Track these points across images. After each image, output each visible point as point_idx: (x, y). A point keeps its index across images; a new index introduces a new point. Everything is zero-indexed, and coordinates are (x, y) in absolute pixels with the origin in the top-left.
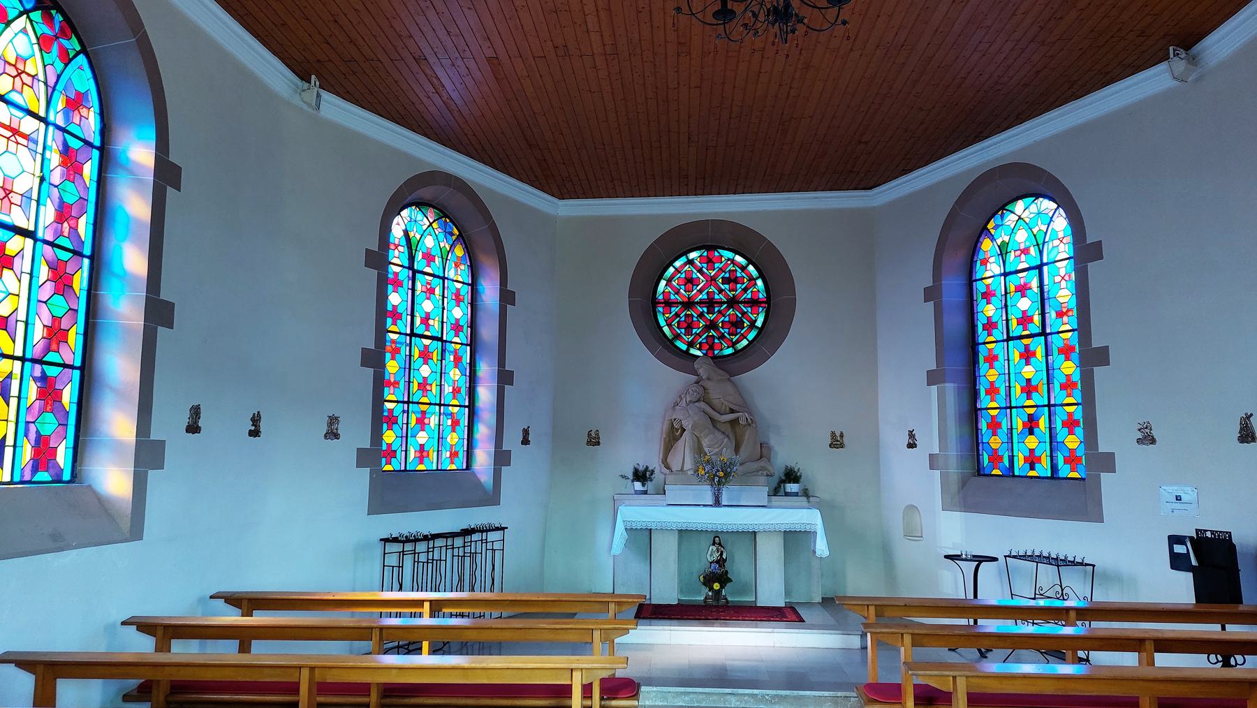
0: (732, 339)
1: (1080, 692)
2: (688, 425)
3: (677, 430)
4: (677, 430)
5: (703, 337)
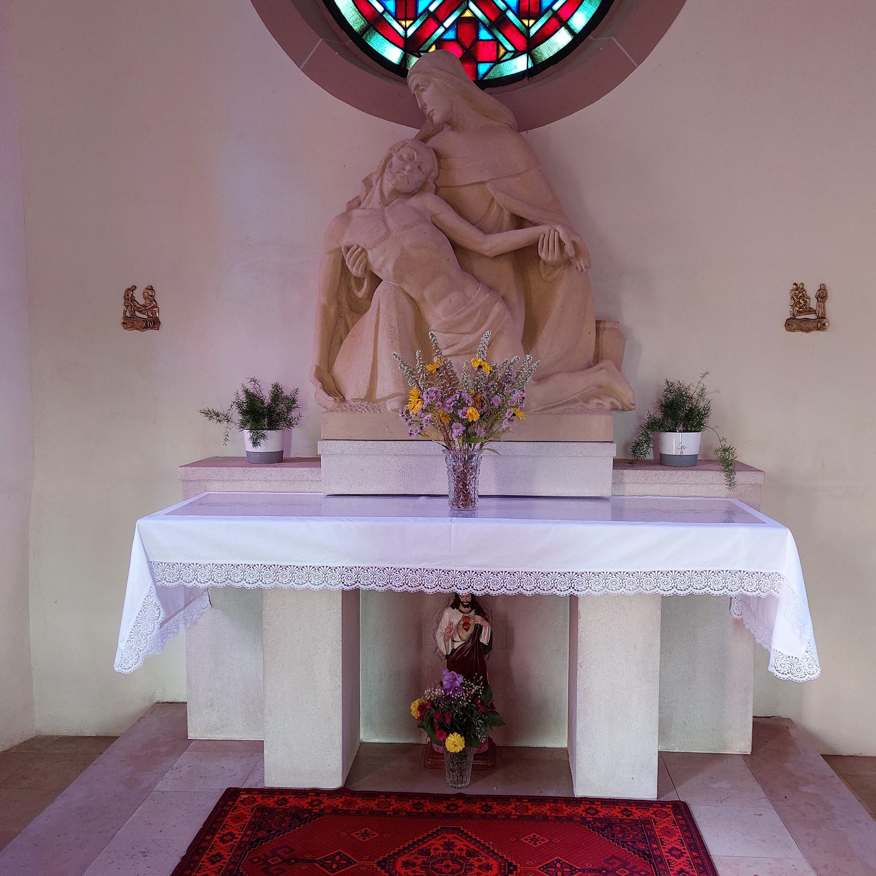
0: (528, 28)
1: (409, 76)
2: (384, 263)
3: (359, 282)
4: (359, 282)
5: (447, 23)
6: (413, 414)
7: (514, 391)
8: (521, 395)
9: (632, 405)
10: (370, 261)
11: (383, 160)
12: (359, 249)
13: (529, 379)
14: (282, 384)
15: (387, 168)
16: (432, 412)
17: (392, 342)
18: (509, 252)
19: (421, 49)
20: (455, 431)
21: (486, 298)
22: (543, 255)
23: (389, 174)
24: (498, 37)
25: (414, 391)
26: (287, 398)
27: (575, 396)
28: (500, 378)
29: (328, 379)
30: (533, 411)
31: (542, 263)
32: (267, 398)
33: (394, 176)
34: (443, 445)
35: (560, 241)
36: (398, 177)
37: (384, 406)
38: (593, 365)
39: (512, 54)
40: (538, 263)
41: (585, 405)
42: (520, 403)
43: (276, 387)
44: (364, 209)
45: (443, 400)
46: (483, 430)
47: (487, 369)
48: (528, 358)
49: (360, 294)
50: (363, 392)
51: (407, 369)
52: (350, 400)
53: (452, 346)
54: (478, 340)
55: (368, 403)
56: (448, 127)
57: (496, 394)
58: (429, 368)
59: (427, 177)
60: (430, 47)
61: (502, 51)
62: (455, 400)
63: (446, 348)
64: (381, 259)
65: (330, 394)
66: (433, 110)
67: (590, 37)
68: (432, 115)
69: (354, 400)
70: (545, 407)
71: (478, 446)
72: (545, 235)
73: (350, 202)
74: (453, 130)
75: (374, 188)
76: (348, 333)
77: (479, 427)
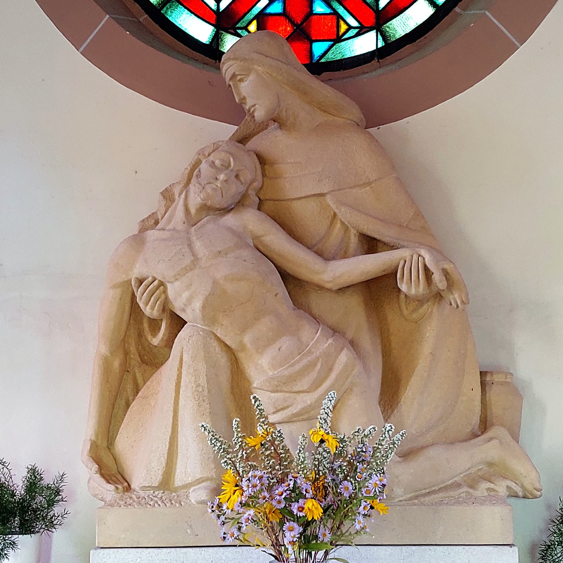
2: (190, 300)
3: (155, 325)
4: (155, 325)
6: (228, 508)
7: (371, 474)
8: (380, 481)
9: (538, 490)
10: (170, 297)
11: (189, 168)
12: (156, 283)
13: (391, 456)
14: (40, 467)
15: (194, 178)
16: (255, 506)
17: (199, 406)
18: (360, 283)
19: (238, 26)
20: (287, 534)
21: (329, 344)
22: (403, 287)
23: (197, 185)
24: (338, 10)
25: (230, 475)
26: (49, 488)
27: (455, 479)
28: (350, 456)
29: (108, 460)
30: (398, 499)
31: (402, 296)
32: (20, 487)
33: (204, 188)
34: (271, 555)
35: (426, 269)
36: (209, 189)
37: (185, 497)
38: (480, 433)
39: (357, 30)
40: (398, 296)
41: (471, 490)
42: (379, 492)
43: (33, 471)
44: (163, 229)
45: (270, 488)
46: (327, 532)
47: (332, 445)
48: (388, 428)
49: (156, 340)
50: (156, 478)
51: (221, 446)
52: (137, 489)
53: (283, 409)
54: (318, 404)
55: (163, 493)
56: (274, 124)
57: (345, 479)
58: (251, 441)
59: (248, 189)
60: (250, 23)
61: (343, 27)
62: (287, 490)
63: (274, 413)
64: (186, 295)
65: (110, 481)
66: (255, 105)
67: (457, 9)
68: (253, 111)
69: (144, 488)
70: (416, 493)
71: (321, 554)
72: (405, 261)
73: (144, 220)
74: (281, 129)
75: (176, 202)
76: (137, 393)
77: (322, 526)
